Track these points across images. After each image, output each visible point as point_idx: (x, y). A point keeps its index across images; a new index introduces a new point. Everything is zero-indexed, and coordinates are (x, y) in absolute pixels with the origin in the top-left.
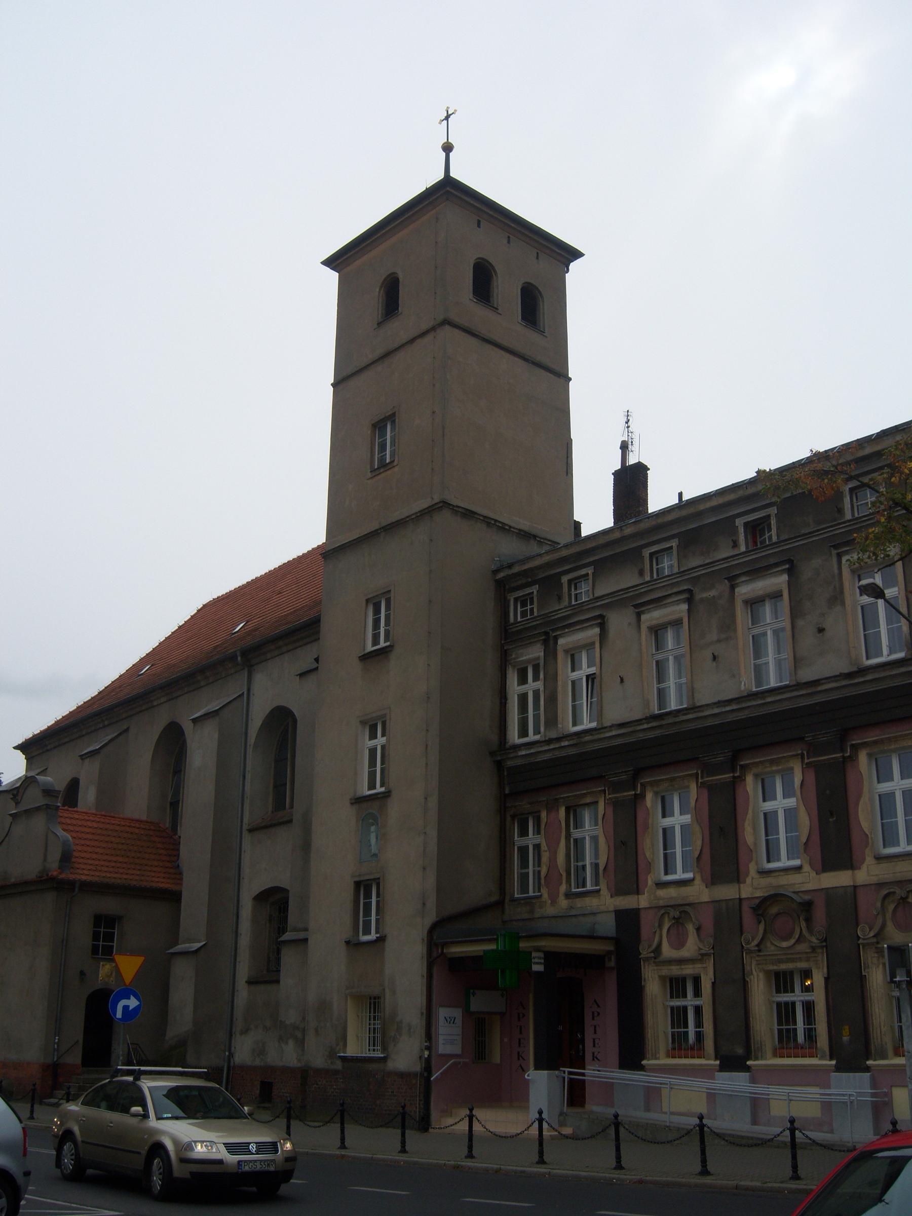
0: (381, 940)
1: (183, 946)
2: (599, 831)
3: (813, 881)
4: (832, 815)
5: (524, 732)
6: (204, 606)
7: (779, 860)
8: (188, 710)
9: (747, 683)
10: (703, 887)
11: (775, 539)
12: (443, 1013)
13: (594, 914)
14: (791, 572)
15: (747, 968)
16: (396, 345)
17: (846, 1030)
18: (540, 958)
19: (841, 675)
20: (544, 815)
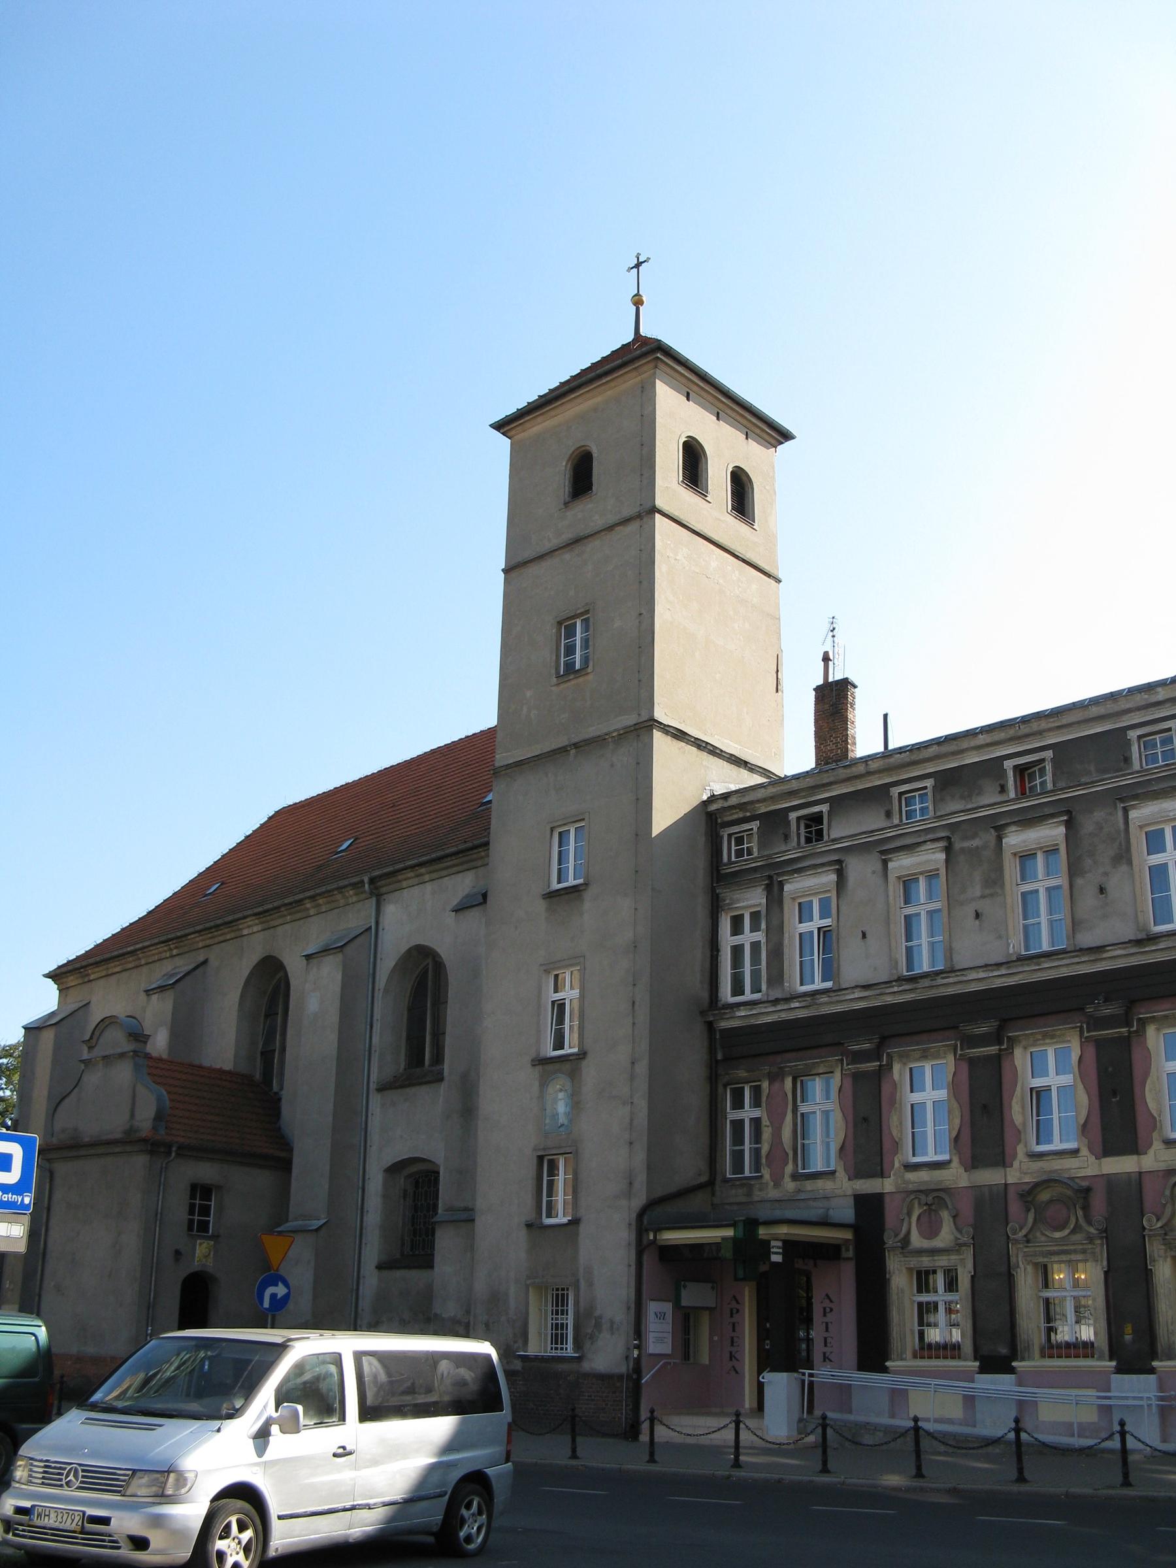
0: (575, 1222)
1: (295, 1223)
2: (833, 1105)
3: (1089, 1166)
4: (1115, 1094)
5: (738, 989)
6: (277, 812)
7: (1050, 1142)
8: (298, 942)
9: (1016, 945)
10: (961, 1170)
11: (1050, 786)
12: (653, 1308)
13: (826, 1198)
14: (1069, 824)
15: (1013, 1260)
16: (588, 532)
17: (1128, 1329)
18: (778, 1247)
19: (1130, 941)
20: (765, 1085)
